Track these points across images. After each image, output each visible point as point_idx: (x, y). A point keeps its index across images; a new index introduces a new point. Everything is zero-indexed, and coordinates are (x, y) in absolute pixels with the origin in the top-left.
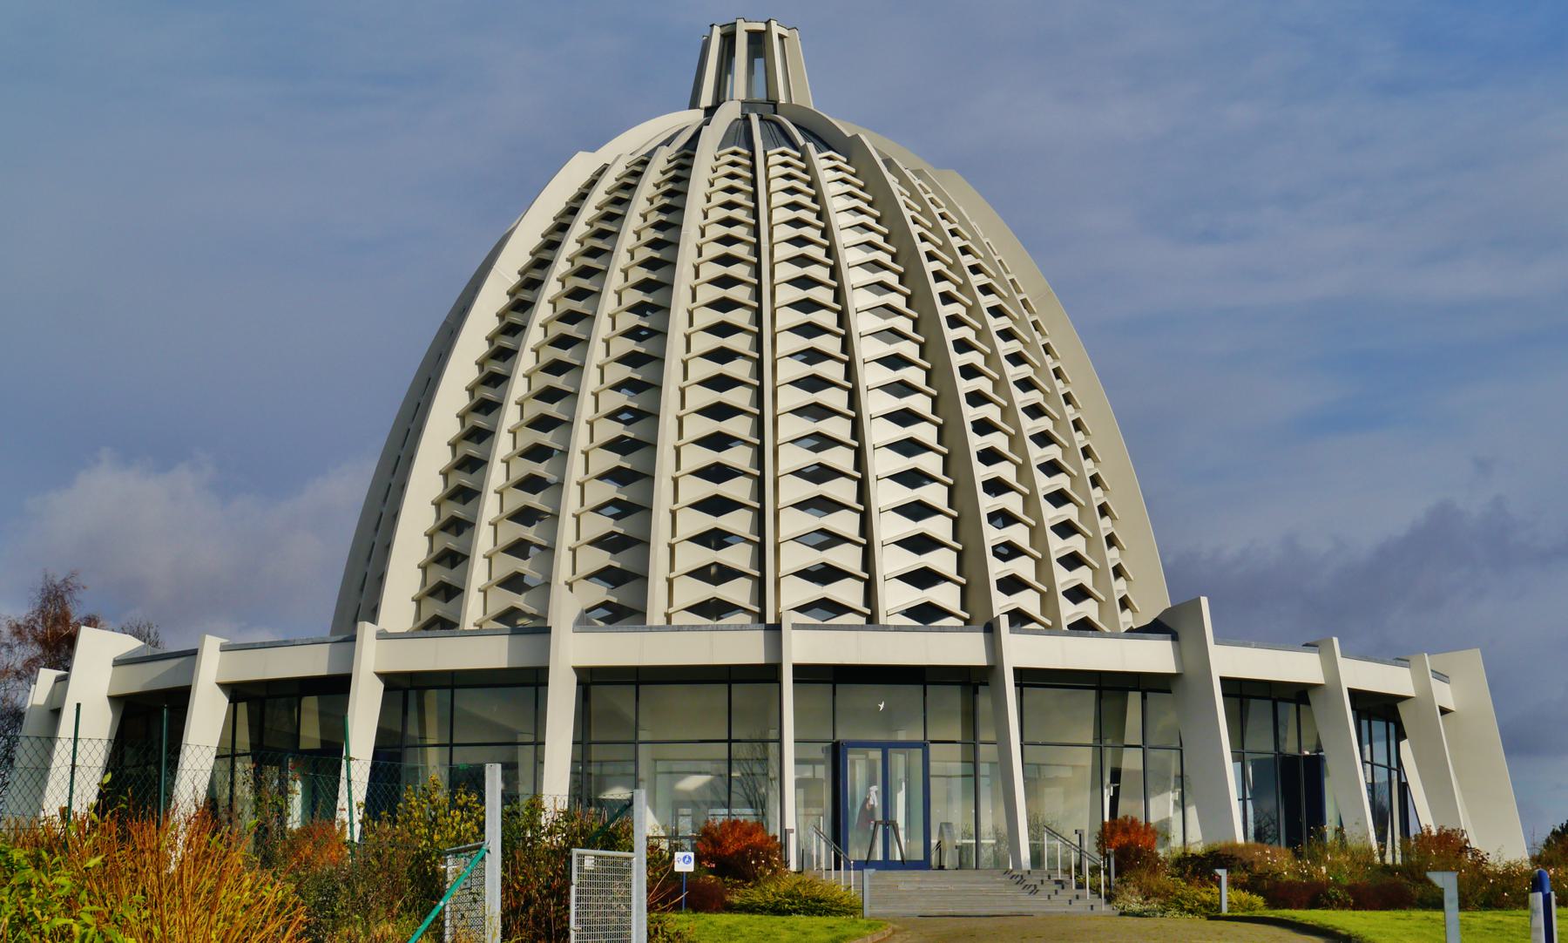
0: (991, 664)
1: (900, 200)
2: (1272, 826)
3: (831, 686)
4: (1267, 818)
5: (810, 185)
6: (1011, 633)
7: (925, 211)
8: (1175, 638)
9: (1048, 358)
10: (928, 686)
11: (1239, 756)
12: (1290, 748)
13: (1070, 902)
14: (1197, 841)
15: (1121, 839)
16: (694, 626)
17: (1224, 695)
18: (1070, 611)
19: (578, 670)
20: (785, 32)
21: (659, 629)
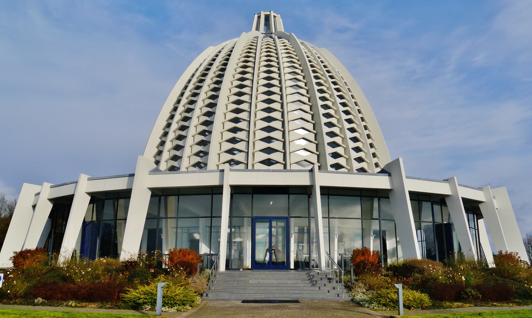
0: (311, 184)
2: (433, 248)
3: (251, 195)
4: (431, 246)
6: (319, 172)
8: (390, 175)
10: (290, 195)
11: (418, 228)
12: (438, 220)
13: (329, 292)
14: (401, 258)
15: (360, 258)
16: (193, 171)
17: (411, 200)
19: (151, 189)
20: (276, 15)
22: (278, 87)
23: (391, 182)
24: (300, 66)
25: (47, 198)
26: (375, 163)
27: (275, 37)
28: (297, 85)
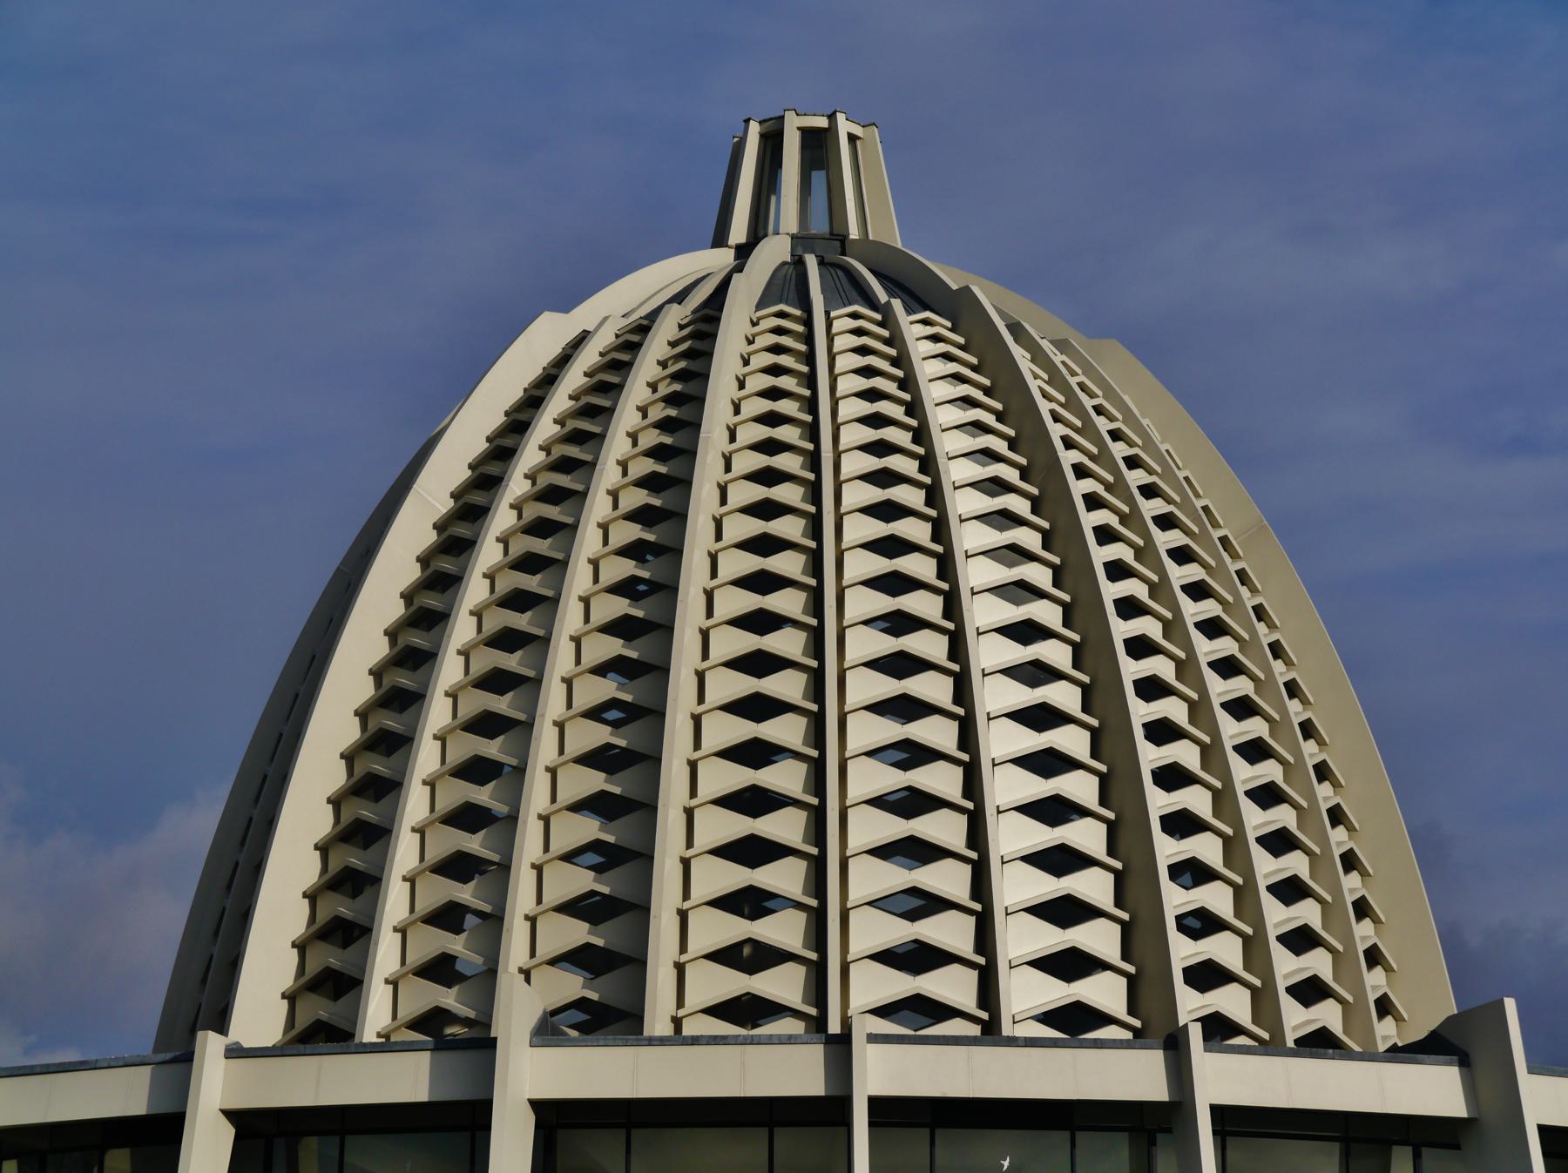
1: (1034, 386)
5: (895, 362)
7: (1072, 403)
8: (1464, 1062)
9: (1261, 628)
18: (1296, 1018)
20: (857, 130)
21: (662, 1041)
22: (935, 590)
23: (1471, 1090)
24: (1000, 417)
25: (218, 1107)
26: (1313, 766)
27: (889, 302)
28: (1013, 548)
